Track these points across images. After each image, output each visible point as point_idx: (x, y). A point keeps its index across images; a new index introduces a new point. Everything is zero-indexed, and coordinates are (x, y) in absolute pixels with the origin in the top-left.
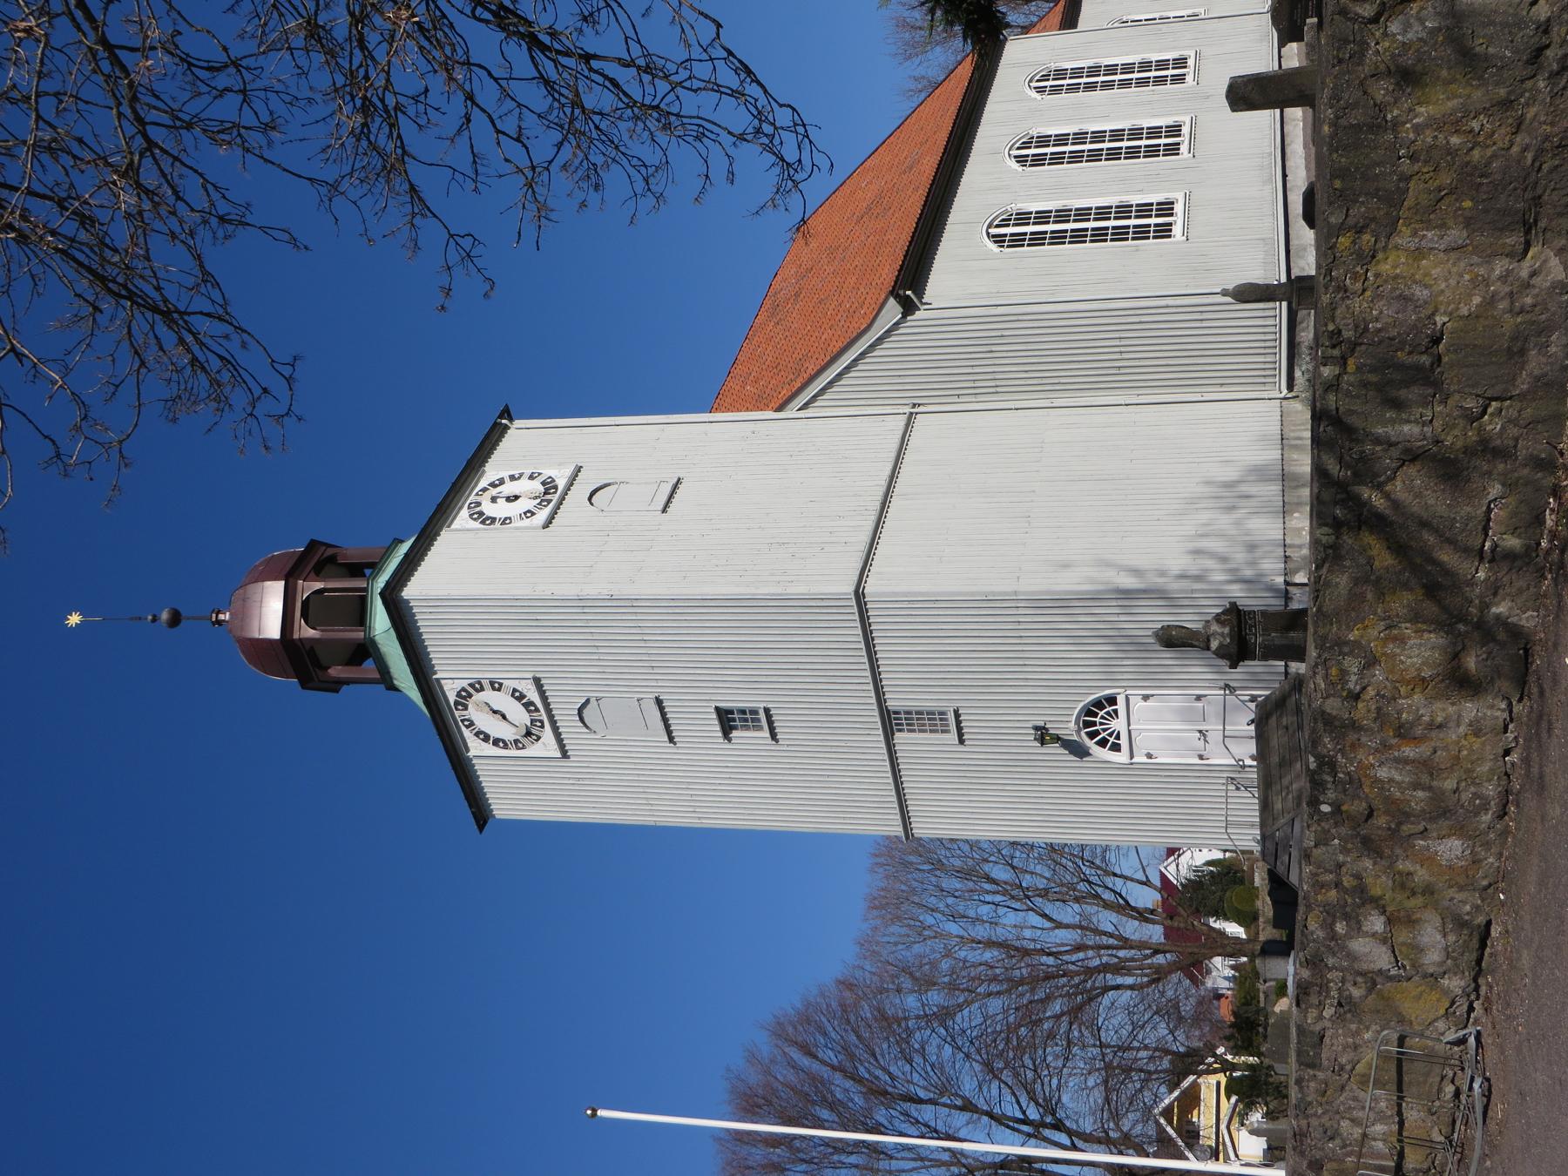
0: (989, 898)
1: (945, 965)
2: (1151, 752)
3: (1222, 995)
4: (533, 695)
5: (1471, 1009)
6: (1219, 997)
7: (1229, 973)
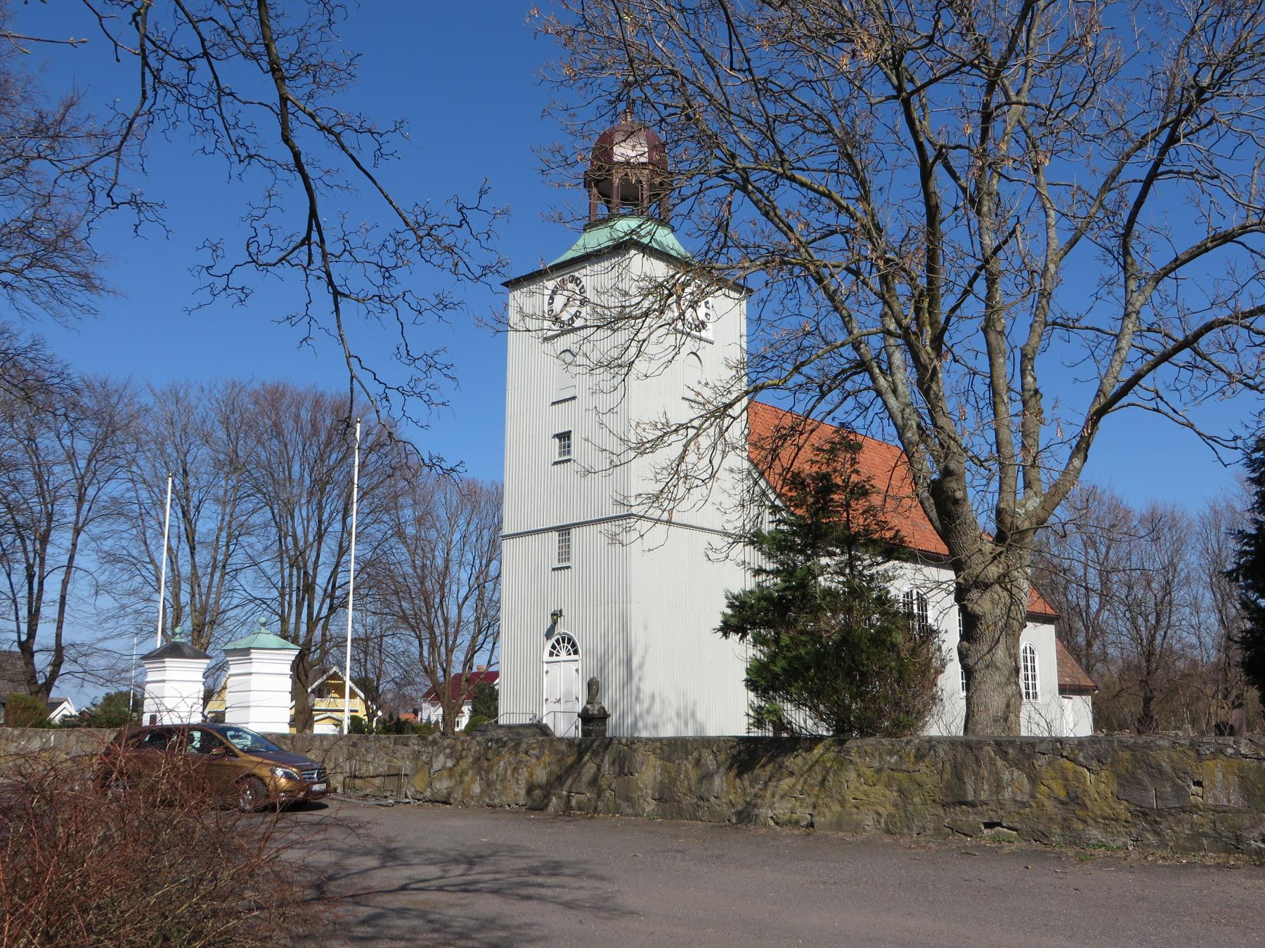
0: (477, 562)
1: (433, 534)
3: (417, 715)
5: (419, 800)
6: (416, 712)
7: (433, 719)
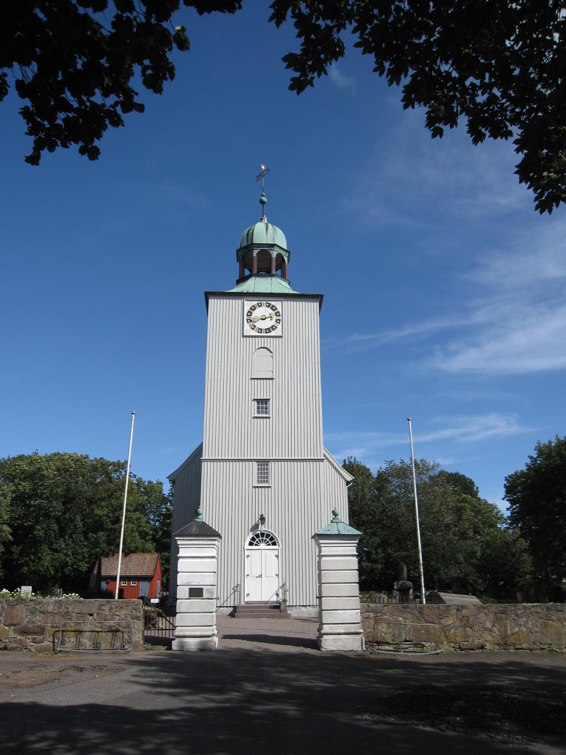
2: (250, 557)
4: (273, 333)
